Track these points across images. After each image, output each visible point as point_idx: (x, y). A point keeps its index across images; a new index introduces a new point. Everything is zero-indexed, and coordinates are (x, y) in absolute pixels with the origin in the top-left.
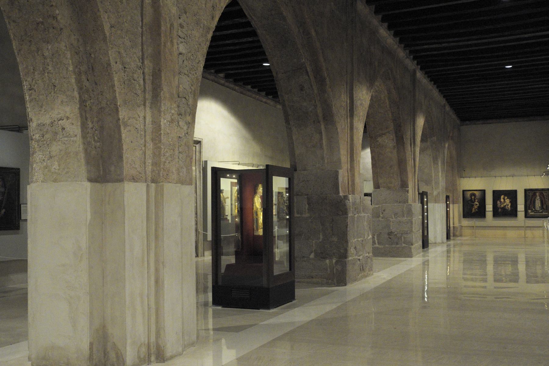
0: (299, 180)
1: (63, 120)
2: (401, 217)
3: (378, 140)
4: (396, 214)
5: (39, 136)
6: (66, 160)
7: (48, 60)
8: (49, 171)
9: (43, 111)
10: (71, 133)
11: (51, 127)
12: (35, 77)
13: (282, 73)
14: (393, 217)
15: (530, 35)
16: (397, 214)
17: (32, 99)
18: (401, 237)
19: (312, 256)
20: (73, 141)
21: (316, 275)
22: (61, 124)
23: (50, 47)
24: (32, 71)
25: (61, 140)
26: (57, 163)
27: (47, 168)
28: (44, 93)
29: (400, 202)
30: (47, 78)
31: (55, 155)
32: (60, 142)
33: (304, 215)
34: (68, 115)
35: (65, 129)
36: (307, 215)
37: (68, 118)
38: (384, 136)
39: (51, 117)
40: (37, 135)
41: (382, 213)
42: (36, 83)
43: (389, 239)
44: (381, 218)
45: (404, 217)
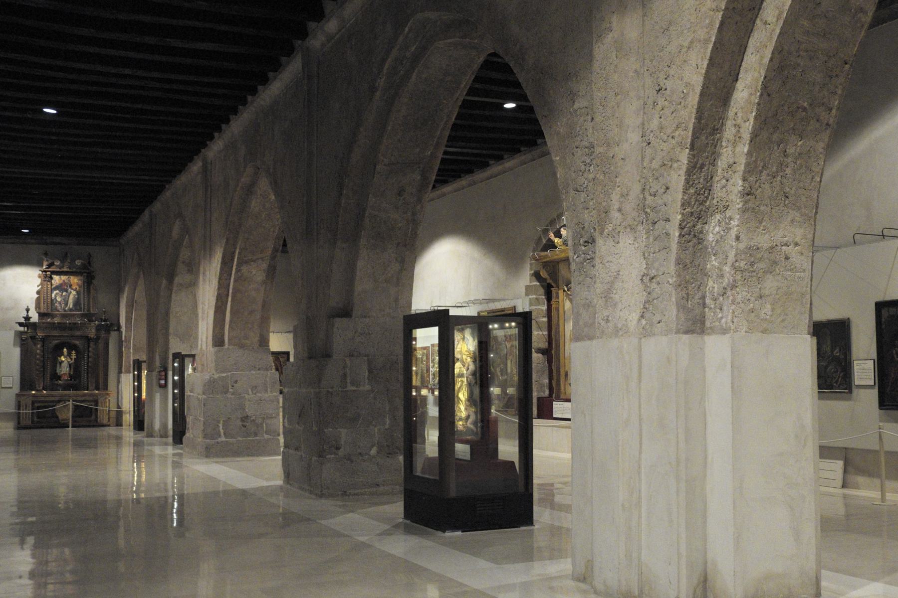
0: (355, 333)
1: (788, 246)
2: (261, 393)
3: (242, 268)
4: (254, 388)
5: (745, 263)
6: (785, 302)
7: (790, 160)
8: (757, 316)
9: (762, 228)
10: (798, 266)
11: (770, 253)
12: (762, 178)
13: (385, 165)
14: (250, 393)
15: (470, 151)
16: (256, 387)
17: (748, 208)
18: (262, 424)
19: (374, 451)
20: (800, 278)
21: (384, 481)
22: (785, 252)
23: (800, 143)
24: (761, 168)
25: (781, 273)
26: (769, 306)
27: (753, 312)
28: (769, 204)
29: (259, 369)
30: (778, 183)
31: (769, 294)
32: (780, 276)
33: (361, 388)
34: (797, 239)
35: (789, 258)
36: (367, 387)
37: (796, 244)
38: (252, 263)
39: (772, 239)
40: (742, 262)
41: (233, 386)
42: (760, 187)
43: (243, 428)
44: (231, 394)
45: (267, 392)
